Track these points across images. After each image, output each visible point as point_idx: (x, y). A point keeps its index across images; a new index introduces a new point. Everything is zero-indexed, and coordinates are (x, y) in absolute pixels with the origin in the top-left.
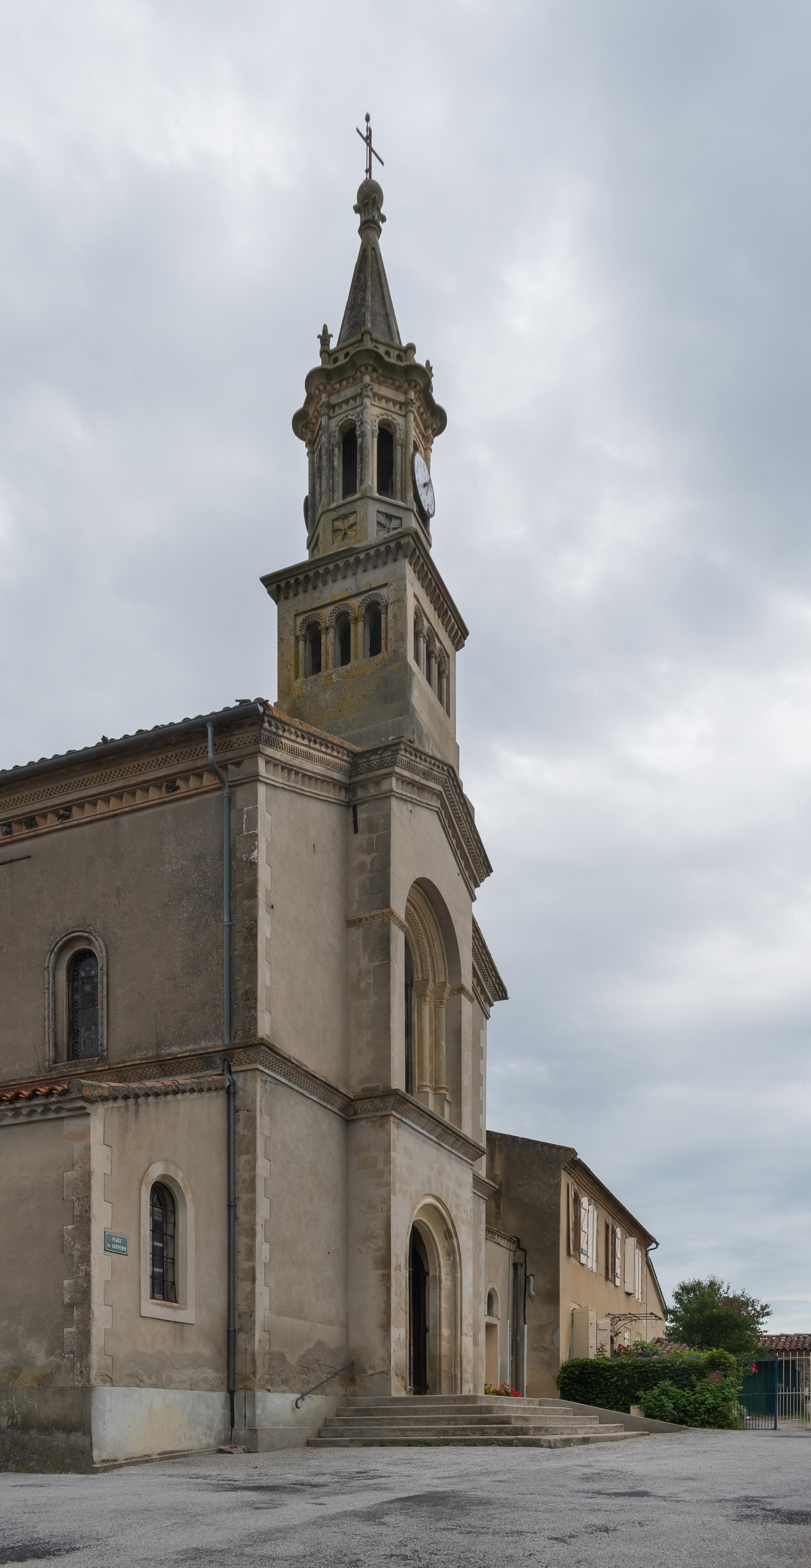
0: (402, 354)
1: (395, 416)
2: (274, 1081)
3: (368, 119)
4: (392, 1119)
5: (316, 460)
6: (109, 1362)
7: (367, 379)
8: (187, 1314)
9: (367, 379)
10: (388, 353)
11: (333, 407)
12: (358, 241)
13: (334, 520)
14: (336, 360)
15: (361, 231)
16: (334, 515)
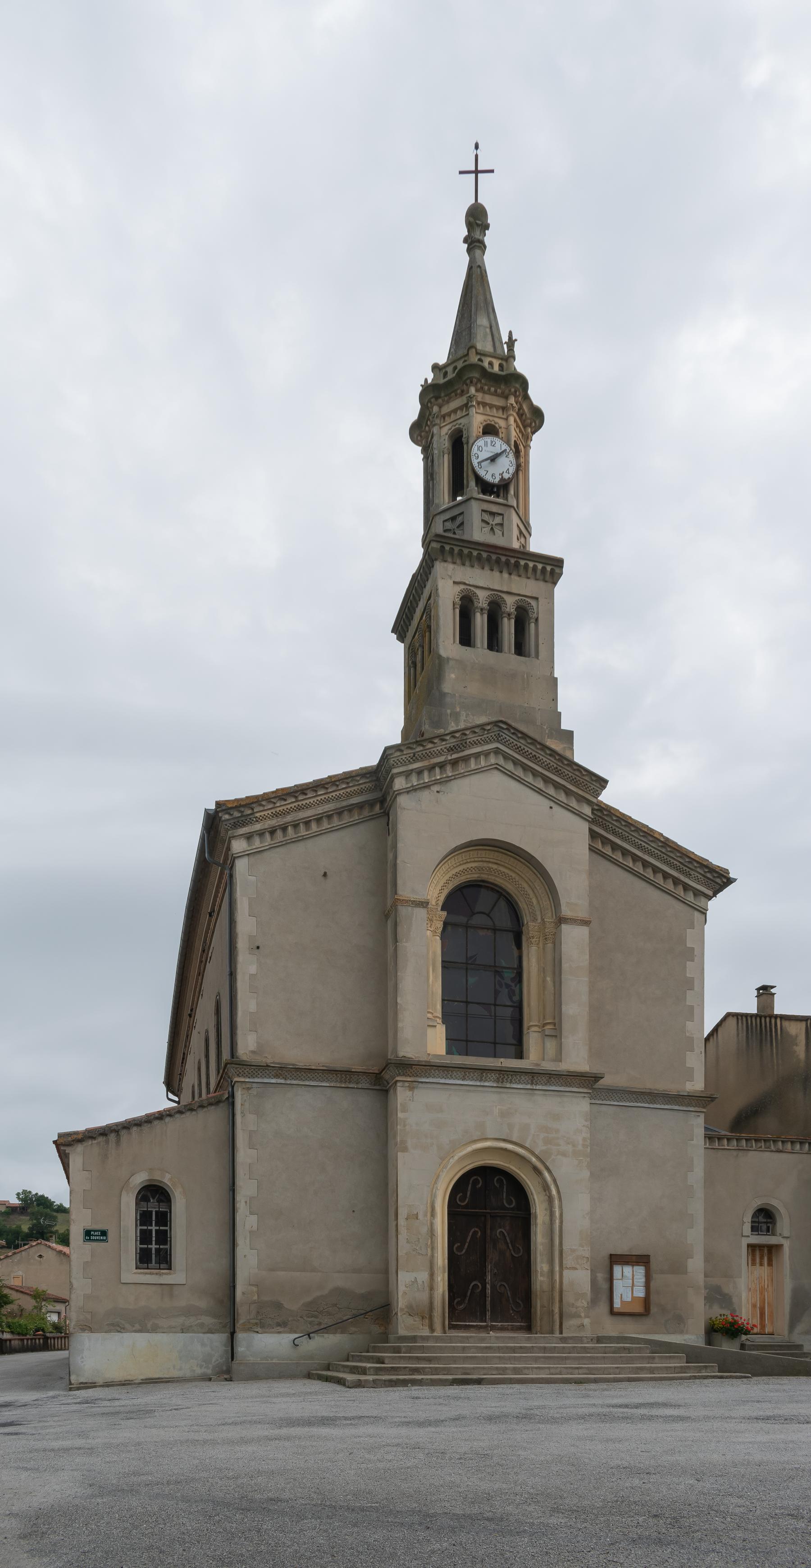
0: (504, 363)
1: (496, 420)
2: (261, 1085)
3: (477, 147)
4: (399, 1084)
5: (430, 464)
6: (89, 1317)
7: (472, 390)
8: (176, 1276)
9: (472, 390)
10: (491, 364)
11: (444, 417)
12: (467, 259)
13: (444, 521)
14: (446, 374)
15: (469, 251)
16: (448, 515)
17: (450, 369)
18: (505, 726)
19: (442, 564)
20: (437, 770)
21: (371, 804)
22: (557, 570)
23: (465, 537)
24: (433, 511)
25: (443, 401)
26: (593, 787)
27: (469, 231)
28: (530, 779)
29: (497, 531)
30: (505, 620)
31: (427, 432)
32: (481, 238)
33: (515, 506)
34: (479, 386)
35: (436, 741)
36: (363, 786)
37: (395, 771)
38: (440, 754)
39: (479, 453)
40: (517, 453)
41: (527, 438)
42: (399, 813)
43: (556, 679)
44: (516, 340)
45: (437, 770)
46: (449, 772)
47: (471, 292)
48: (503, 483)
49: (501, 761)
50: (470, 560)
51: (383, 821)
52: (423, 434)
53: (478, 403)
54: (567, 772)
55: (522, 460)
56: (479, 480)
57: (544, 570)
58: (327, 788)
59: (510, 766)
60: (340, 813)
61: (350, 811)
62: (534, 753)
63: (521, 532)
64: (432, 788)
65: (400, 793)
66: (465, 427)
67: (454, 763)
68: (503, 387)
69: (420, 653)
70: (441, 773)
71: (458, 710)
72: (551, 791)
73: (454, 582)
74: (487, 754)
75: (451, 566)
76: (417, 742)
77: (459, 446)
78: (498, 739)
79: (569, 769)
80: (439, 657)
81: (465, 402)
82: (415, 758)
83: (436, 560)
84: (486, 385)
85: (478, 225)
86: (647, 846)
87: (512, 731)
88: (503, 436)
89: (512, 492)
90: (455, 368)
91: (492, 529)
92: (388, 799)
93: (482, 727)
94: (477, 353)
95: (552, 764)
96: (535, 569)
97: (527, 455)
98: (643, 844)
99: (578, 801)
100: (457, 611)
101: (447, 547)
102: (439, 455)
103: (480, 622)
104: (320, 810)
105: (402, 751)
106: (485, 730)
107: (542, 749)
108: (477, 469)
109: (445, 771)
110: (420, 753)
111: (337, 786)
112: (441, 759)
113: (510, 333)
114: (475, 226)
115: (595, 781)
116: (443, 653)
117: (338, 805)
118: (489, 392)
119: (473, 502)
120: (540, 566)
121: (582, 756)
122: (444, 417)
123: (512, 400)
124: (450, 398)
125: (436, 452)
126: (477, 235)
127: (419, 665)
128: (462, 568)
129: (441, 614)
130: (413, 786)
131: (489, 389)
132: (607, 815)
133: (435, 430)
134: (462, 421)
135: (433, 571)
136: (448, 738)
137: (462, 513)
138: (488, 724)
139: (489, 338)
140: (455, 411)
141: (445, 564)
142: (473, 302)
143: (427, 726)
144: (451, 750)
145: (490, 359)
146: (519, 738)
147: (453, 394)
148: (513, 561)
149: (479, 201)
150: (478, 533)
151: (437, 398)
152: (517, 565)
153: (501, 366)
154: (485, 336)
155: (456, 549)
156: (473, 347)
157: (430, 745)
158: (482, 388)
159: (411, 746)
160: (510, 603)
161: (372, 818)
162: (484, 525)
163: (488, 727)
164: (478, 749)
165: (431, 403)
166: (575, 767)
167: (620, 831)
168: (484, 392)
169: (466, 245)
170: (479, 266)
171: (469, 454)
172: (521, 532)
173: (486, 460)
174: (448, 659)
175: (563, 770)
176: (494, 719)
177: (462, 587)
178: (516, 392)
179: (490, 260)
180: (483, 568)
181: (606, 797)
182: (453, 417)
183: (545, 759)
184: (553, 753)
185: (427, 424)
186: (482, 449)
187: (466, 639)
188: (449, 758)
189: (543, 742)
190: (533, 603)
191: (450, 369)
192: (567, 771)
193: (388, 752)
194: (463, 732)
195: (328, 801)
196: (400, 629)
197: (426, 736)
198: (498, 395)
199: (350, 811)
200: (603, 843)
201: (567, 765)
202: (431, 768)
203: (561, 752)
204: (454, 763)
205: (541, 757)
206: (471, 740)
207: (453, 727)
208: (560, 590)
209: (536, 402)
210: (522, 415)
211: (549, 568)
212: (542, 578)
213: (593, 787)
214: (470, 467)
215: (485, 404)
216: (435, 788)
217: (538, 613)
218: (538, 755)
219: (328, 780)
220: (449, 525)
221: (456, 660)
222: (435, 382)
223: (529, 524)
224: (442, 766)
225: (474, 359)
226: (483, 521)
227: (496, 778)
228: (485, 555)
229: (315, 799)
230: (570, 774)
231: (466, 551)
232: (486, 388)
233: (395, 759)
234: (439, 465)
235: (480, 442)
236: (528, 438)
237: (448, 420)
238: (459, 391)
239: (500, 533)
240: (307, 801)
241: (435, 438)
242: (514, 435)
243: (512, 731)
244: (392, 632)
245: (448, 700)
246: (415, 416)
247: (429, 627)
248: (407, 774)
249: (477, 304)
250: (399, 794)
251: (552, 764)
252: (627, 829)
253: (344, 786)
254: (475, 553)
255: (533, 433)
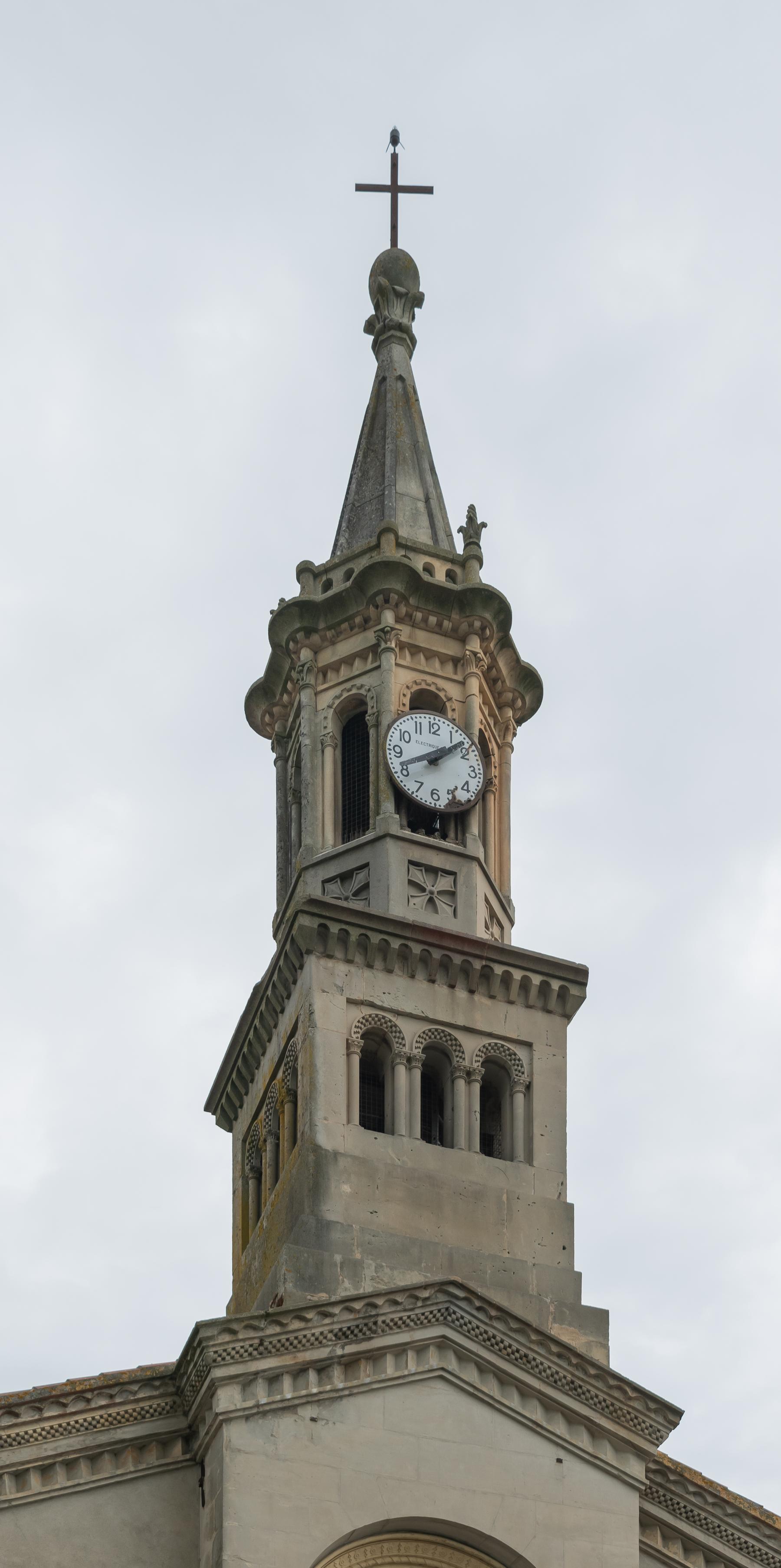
0: (458, 570)
1: (441, 683)
3: (395, 139)
5: (291, 770)
7: (389, 617)
9: (389, 617)
10: (428, 569)
11: (324, 672)
12: (372, 365)
13: (325, 882)
14: (328, 585)
15: (377, 347)
16: (332, 870)
17: (337, 576)
18: (461, 1294)
19: (323, 962)
20: (312, 1376)
21: (164, 1442)
22: (574, 990)
23: (374, 910)
24: (298, 861)
25: (324, 638)
26: (649, 1422)
27: (377, 307)
28: (514, 1401)
29: (442, 904)
30: (461, 1084)
31: (285, 706)
32: (405, 321)
33: (482, 857)
34: (403, 610)
35: (310, 1315)
36: (145, 1404)
37: (218, 1373)
38: (318, 1341)
39: (402, 744)
40: (485, 755)
41: (506, 731)
42: (227, 1459)
43: (571, 1206)
44: (484, 525)
45: (312, 1376)
46: (338, 1379)
47: (384, 427)
48: (455, 810)
49: (452, 1364)
50: (385, 959)
51: (192, 1476)
52: (276, 710)
53: (402, 646)
54: (594, 1392)
55: (495, 772)
56: (404, 802)
57: (544, 988)
58: (65, 1405)
59: (471, 1375)
60: (93, 1457)
61: (116, 1454)
62: (524, 1350)
63: (493, 915)
64: (300, 1411)
65: (228, 1418)
66: (373, 693)
67: (350, 1364)
68: (455, 616)
69: (269, 1147)
70: (320, 1383)
71: (358, 1256)
72: (560, 1427)
73: (350, 1001)
74: (421, 1349)
75: (341, 968)
76: (267, 1316)
77: (357, 733)
78: (446, 1318)
79: (599, 1384)
80: (317, 1149)
81: (373, 641)
82: (262, 1349)
83: (309, 952)
84: (418, 608)
85: (398, 295)
86: (758, 1545)
87: (478, 1303)
88: (456, 716)
89: (474, 828)
90: (348, 575)
91: (431, 901)
92: (202, 1433)
93: (411, 1291)
94: (399, 545)
95: (562, 1373)
96: (525, 984)
97: (505, 763)
98: (751, 1542)
99: (617, 1450)
100: (356, 1059)
101: (334, 928)
102: (314, 750)
103: (405, 1087)
104: (49, 1449)
105: (233, 1332)
106: (417, 1298)
107: (540, 1343)
108: (399, 777)
109: (330, 1378)
110: (274, 1340)
111: (88, 1401)
112: (322, 1353)
113: (472, 509)
114: (392, 297)
115: (655, 1411)
116: (323, 1140)
117: (90, 1440)
118: (424, 625)
119: (390, 844)
120: (536, 980)
121: (630, 1355)
122: (324, 672)
123: (475, 645)
124: (339, 634)
125: (305, 741)
126: (396, 313)
127: (285, 1134)
128: (367, 973)
129: (319, 1061)
130: (258, 1406)
131: (425, 620)
132: (675, 1482)
133: (305, 697)
134: (365, 680)
135: (303, 977)
136: (336, 1310)
137: (367, 865)
138: (425, 1287)
139: (424, 521)
140: (349, 660)
141: (330, 963)
142: (389, 446)
143: (290, 1286)
144: (342, 1335)
145: (428, 559)
146: (491, 1318)
147: (345, 626)
148: (477, 965)
149: (400, 246)
150: (399, 902)
151: (309, 632)
152: (486, 975)
153: (450, 575)
154: (415, 516)
155: (354, 934)
156: (390, 530)
157: (296, 1325)
158: (409, 616)
159: (255, 1323)
160: (471, 1049)
161: (166, 1470)
162: (413, 892)
163: (425, 1294)
164: (403, 1337)
165: (296, 642)
166: (612, 1382)
167: (703, 1515)
168: (414, 625)
169: (371, 338)
170: (401, 378)
171: (381, 746)
172: (493, 915)
173: (419, 759)
174: (336, 1154)
175: (586, 1387)
176: (439, 1277)
177: (367, 1011)
178: (483, 629)
179: (425, 369)
180: (413, 977)
181: (675, 1447)
182: (344, 672)
183: (547, 1363)
184: (566, 1351)
185: (285, 690)
186: (408, 740)
187: (374, 1114)
188: (339, 1352)
189: (543, 1328)
190: (521, 1053)
191: (337, 576)
192: (596, 1388)
193: (203, 1334)
194: (369, 1299)
195: (67, 1431)
196: (224, 1101)
197: (288, 1305)
198: (445, 635)
199: (116, 1454)
200: (665, 1538)
201: (596, 1377)
202: (299, 1372)
203: (581, 1350)
204: (350, 1364)
205: (539, 1359)
206: (388, 1319)
207: (347, 1288)
208: (580, 1030)
209: (526, 656)
210: (495, 681)
211: (556, 985)
212: (539, 1004)
213: (649, 1422)
214: (382, 773)
215: (415, 650)
216: (308, 1412)
217: (531, 1074)
218: (531, 1355)
219: (68, 1389)
220: (335, 888)
221: (355, 1158)
222: (306, 597)
223: (509, 901)
224: (322, 1368)
225: (390, 552)
226: (411, 883)
227: (442, 1397)
228: (417, 949)
229: (38, 1427)
230: (602, 1396)
231: (375, 938)
232: (419, 615)
233: (220, 1349)
234: (313, 769)
235: (407, 724)
236: (507, 729)
237: (332, 678)
238: (358, 620)
239: (450, 910)
240: (21, 1430)
241: (304, 714)
242: (477, 718)
243: (478, 1303)
244: (207, 1108)
245: (336, 1235)
246: (259, 672)
247: (293, 1095)
248: (247, 1381)
249: (396, 452)
250: (228, 1420)
251: (562, 1373)
252: (718, 1512)
253: (103, 1402)
254: (395, 944)
255: (519, 722)
